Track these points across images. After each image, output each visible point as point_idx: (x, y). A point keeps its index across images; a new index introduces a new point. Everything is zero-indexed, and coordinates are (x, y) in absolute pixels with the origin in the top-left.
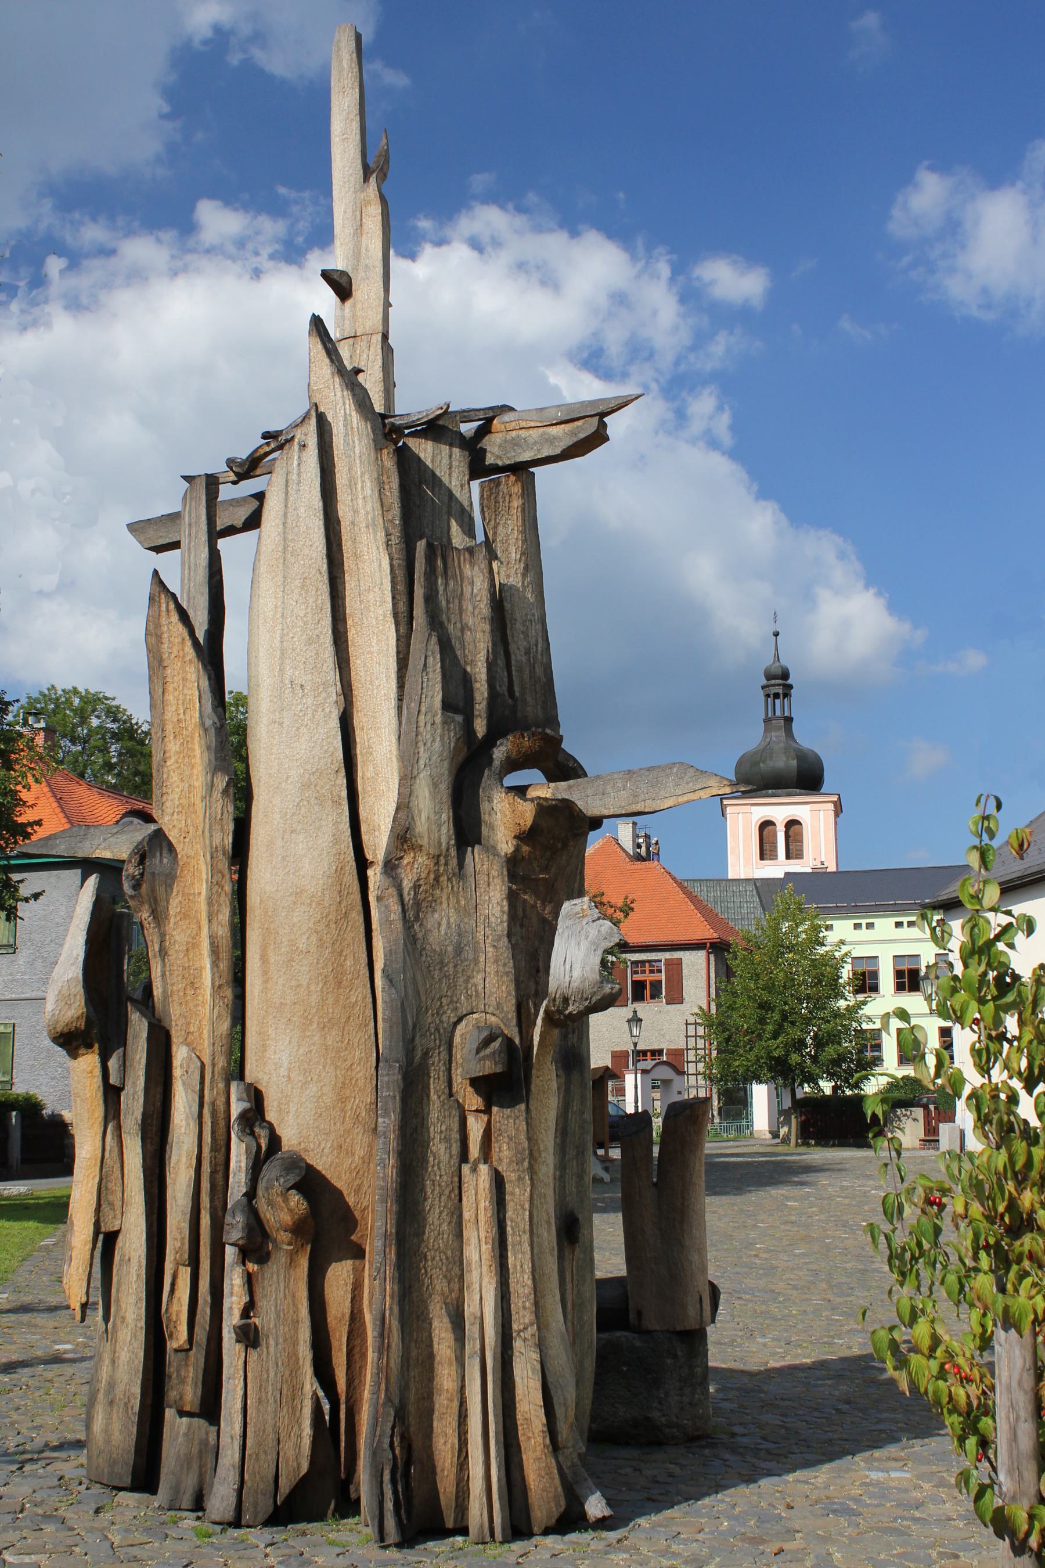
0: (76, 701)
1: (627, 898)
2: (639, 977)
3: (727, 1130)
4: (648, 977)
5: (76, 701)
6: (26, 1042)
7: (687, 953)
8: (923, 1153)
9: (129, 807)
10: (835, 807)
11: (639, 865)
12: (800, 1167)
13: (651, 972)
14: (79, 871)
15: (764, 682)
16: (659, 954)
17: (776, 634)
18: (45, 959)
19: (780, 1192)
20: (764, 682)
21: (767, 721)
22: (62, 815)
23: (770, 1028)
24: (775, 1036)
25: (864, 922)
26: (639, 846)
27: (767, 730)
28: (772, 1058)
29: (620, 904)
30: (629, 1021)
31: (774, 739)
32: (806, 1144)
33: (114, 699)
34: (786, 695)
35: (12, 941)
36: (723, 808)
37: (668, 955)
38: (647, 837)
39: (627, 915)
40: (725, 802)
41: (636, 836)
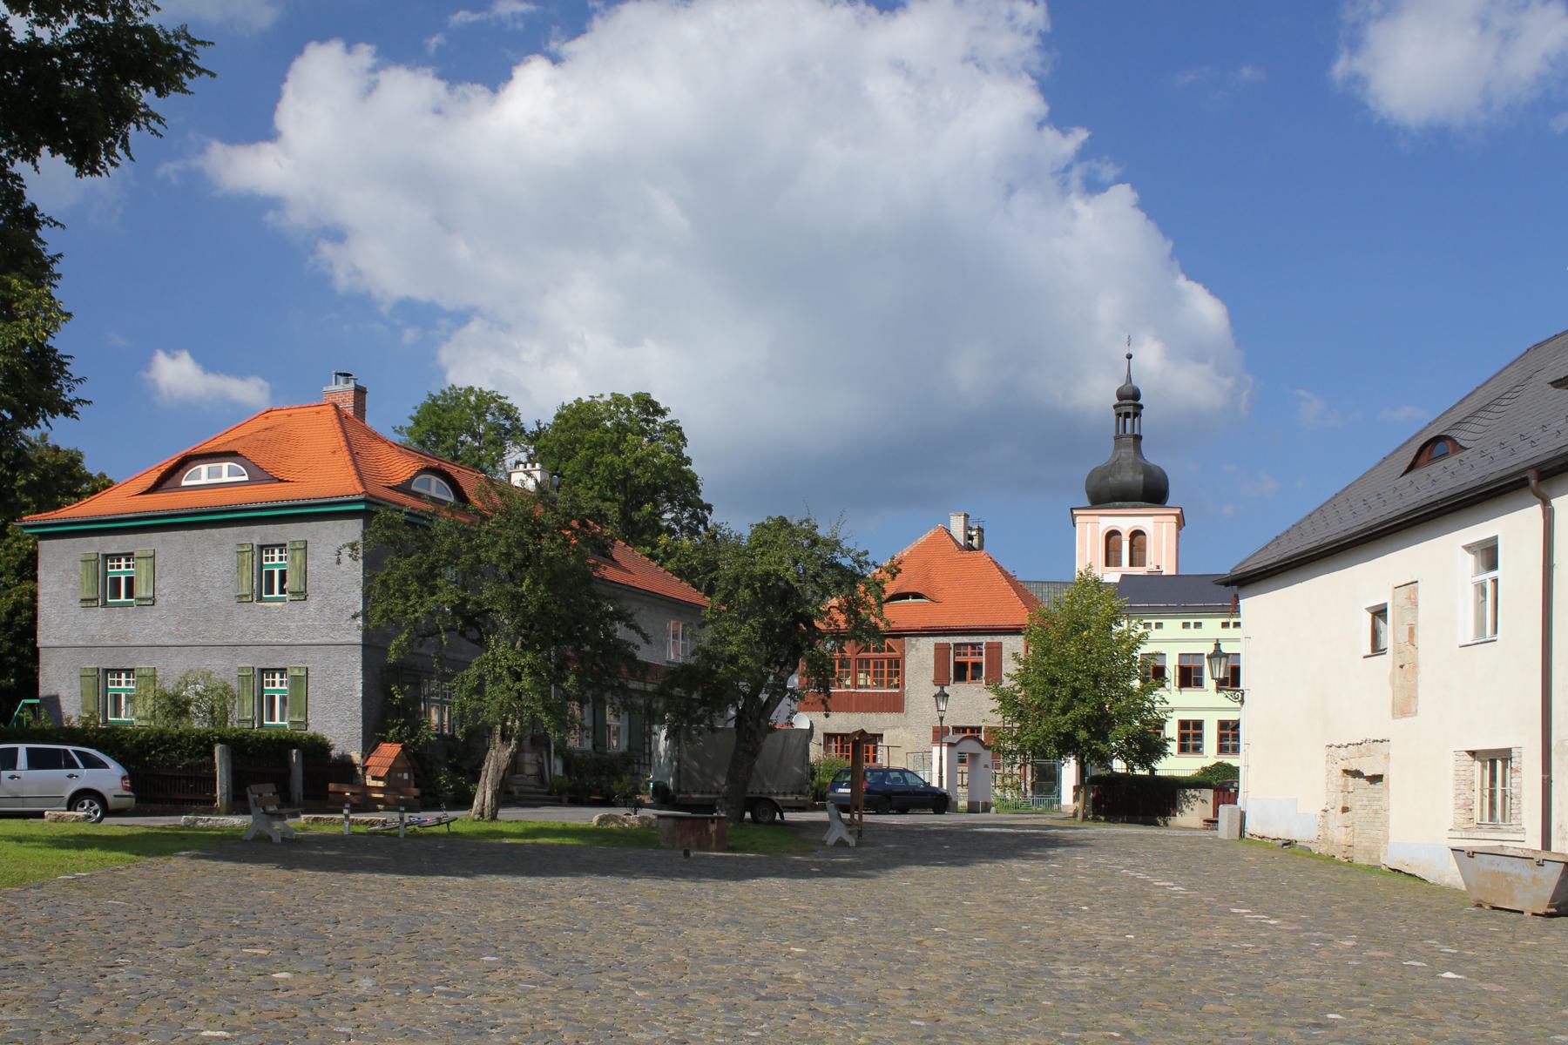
0: (473, 398)
1: (893, 558)
2: (960, 659)
3: (1039, 803)
4: (970, 659)
5: (473, 398)
6: (318, 685)
7: (1008, 637)
8: (1203, 833)
9: (425, 465)
10: (1178, 519)
11: (967, 554)
12: (1065, 841)
13: (973, 654)
14: (361, 521)
15: (1116, 401)
16: (981, 637)
17: (1129, 357)
18: (332, 606)
19: (1024, 866)
20: (1116, 401)
21: (1117, 438)
22: (352, 467)
23: (1060, 704)
24: (1064, 711)
25: (1192, 621)
26: (971, 538)
27: (1117, 447)
28: (1059, 734)
29: (886, 564)
30: (936, 696)
31: (1123, 455)
32: (1095, 820)
33: (506, 398)
34: (1137, 415)
35: (303, 588)
36: (1073, 517)
37: (988, 639)
38: (980, 530)
39: (894, 575)
40: (1075, 512)
41: (967, 528)
